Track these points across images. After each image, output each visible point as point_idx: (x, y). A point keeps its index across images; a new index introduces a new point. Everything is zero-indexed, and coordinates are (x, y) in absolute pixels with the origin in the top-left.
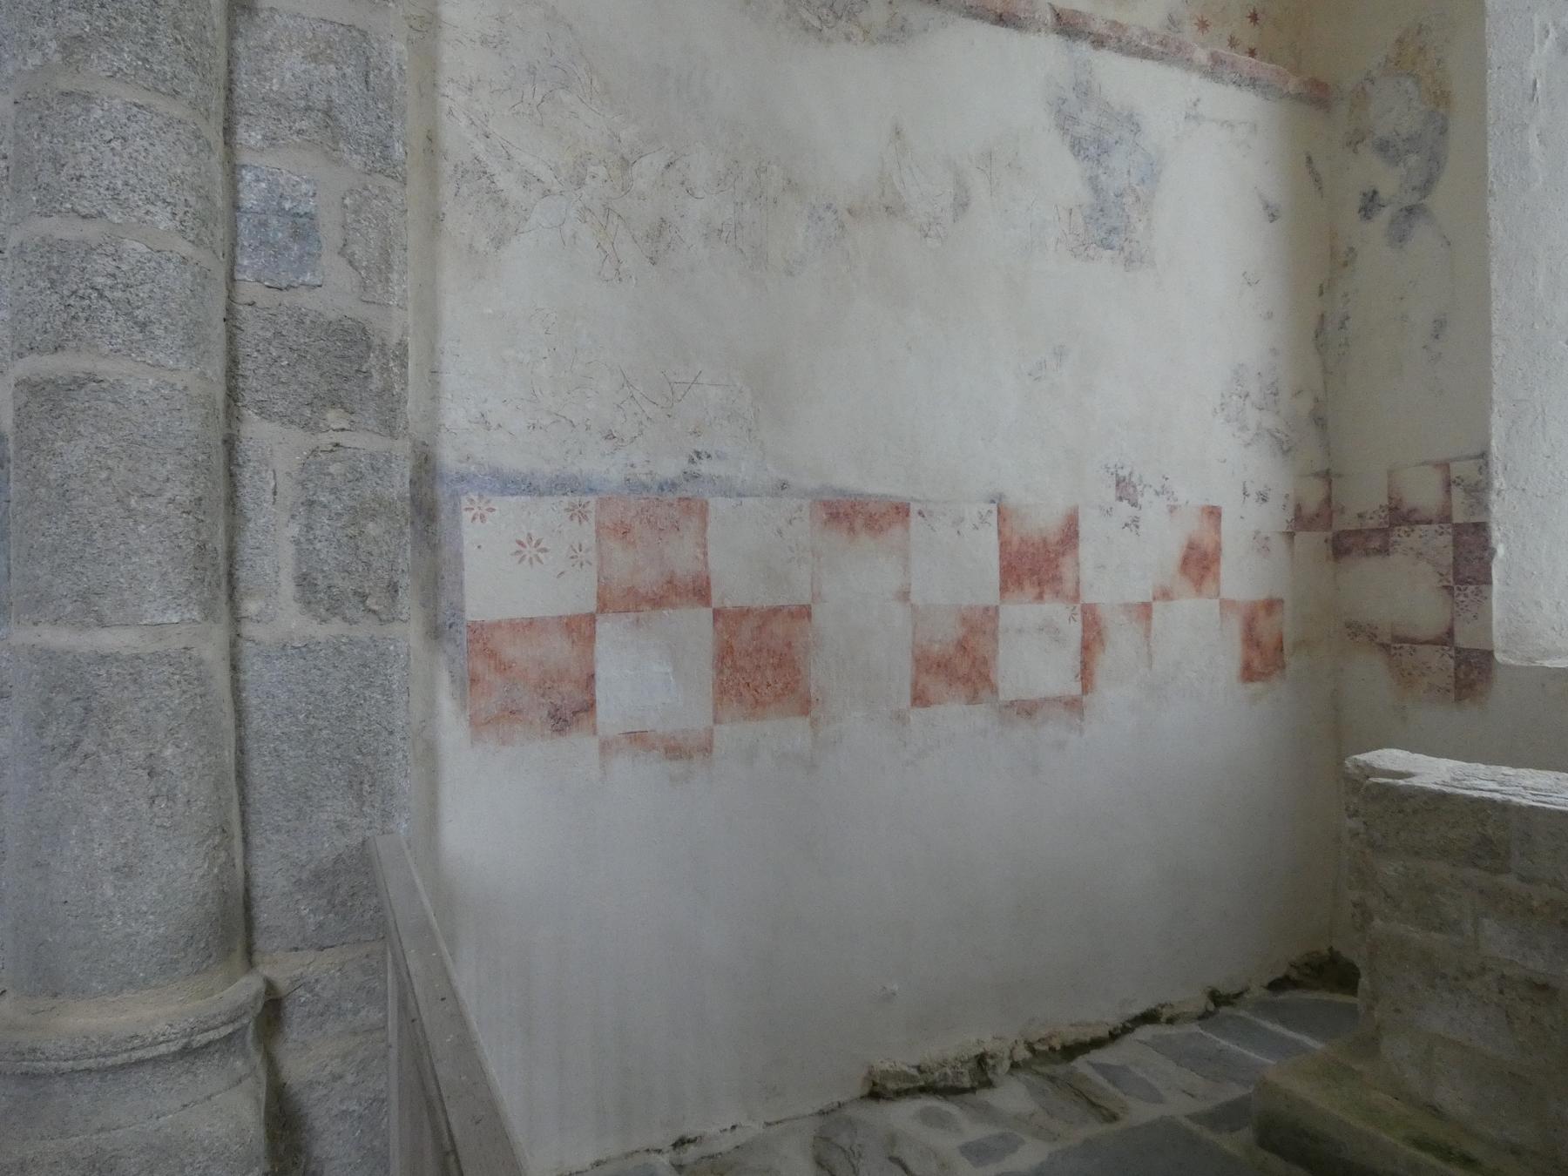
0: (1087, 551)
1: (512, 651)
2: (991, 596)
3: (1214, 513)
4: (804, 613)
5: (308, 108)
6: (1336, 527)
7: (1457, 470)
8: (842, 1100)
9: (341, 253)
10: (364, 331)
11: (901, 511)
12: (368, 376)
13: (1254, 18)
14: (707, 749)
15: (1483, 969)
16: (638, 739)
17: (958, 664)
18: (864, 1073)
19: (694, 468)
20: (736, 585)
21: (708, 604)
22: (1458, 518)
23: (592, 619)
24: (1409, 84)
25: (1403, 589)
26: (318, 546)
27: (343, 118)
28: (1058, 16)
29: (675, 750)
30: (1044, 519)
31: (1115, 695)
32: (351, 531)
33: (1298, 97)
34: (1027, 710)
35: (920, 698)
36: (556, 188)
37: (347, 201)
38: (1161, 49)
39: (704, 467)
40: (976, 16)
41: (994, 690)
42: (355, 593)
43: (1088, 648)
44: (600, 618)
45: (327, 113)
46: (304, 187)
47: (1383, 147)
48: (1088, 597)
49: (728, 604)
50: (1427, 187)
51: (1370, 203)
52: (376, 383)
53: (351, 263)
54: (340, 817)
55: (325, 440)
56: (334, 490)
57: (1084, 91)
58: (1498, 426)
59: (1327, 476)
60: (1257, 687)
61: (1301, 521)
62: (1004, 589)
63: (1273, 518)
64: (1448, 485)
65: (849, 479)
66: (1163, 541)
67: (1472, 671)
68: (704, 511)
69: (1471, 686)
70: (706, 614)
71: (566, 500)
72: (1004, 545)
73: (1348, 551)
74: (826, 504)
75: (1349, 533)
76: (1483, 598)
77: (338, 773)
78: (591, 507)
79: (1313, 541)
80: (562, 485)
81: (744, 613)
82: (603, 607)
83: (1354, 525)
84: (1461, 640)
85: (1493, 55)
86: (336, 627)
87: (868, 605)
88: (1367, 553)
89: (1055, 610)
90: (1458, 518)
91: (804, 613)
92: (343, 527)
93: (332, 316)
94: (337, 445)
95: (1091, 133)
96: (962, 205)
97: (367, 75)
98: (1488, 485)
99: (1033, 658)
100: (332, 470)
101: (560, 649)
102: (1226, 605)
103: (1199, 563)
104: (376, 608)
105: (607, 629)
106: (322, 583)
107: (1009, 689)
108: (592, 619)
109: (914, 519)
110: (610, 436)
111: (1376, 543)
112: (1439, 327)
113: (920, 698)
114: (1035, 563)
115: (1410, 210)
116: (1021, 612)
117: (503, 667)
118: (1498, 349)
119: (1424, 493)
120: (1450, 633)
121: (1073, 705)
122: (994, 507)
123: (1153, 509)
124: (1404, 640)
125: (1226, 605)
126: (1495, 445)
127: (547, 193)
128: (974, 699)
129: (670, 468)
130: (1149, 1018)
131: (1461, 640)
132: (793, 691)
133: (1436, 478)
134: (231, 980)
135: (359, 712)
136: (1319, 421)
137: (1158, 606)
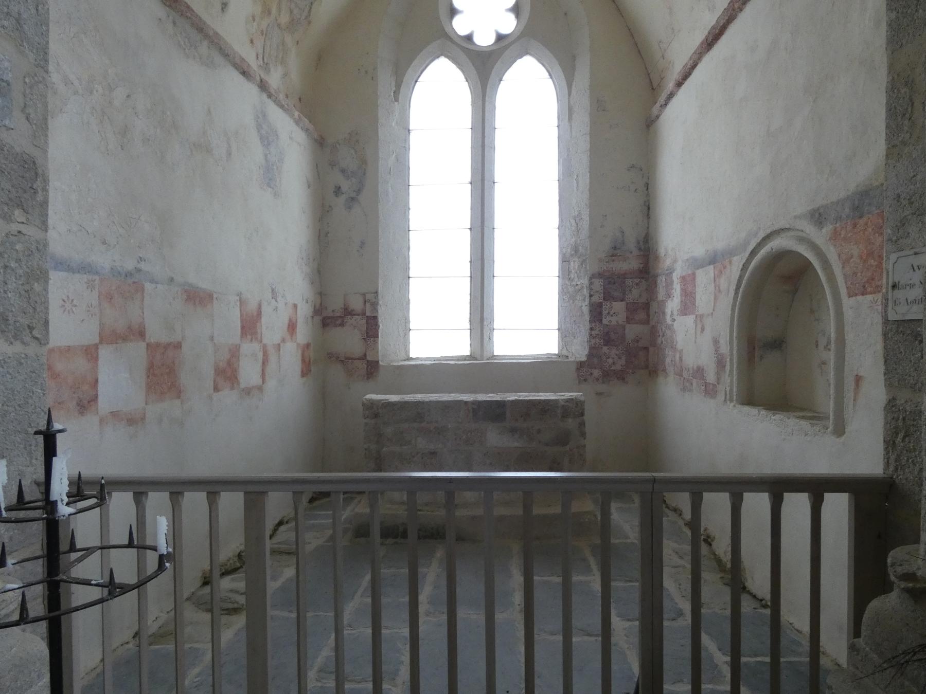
0: (264, 320)
1: (59, 366)
2: (237, 339)
3: (295, 306)
4: (178, 346)
5: (8, 14)
6: (327, 318)
7: (368, 297)
8: (193, 590)
9: (23, 111)
10: (34, 163)
11: (210, 296)
12: (36, 192)
13: (300, 99)
14: (143, 419)
15: (418, 453)
16: (115, 415)
17: (227, 374)
19: (139, 266)
20: (156, 333)
21: (144, 340)
22: (368, 314)
23: (96, 347)
24: (353, 151)
25: (348, 340)
26: (10, 295)
27: (26, 27)
28: (261, 80)
30: (252, 307)
31: (271, 384)
32: (27, 287)
33: (316, 140)
34: (248, 391)
35: (216, 389)
36: (80, 91)
37: (27, 80)
39: (142, 266)
40: (236, 68)
41: (238, 384)
42: (29, 326)
43: (265, 362)
44: (100, 346)
45: (18, 21)
46: (7, 64)
47: (343, 171)
48: (265, 341)
49: (152, 340)
50: (359, 191)
51: (338, 191)
52: (40, 197)
53: (28, 119)
54: (21, 467)
55: (14, 227)
56: (18, 261)
57: (264, 116)
58: (380, 282)
60: (305, 379)
62: (242, 337)
64: (365, 302)
67: (372, 368)
68: (143, 290)
69: (372, 374)
70: (143, 345)
71: (85, 277)
72: (242, 315)
73: (328, 325)
74: (186, 291)
75: (329, 318)
76: (376, 342)
77: (19, 440)
78: (96, 282)
79: (318, 319)
80: (85, 268)
81: (158, 345)
82: (101, 342)
83: (331, 315)
84: (369, 358)
85: (380, 154)
86: (18, 348)
88: (336, 326)
89: (255, 347)
90: (368, 314)
92: (22, 285)
93: (18, 149)
94: (20, 232)
97: (37, 6)
98: (377, 304)
100: (17, 247)
101: (80, 364)
102: (298, 345)
103: (292, 327)
104: (38, 336)
105: (105, 353)
106: (11, 319)
108: (96, 347)
109: (215, 301)
110: (104, 243)
111: (339, 322)
112: (362, 245)
113: (216, 389)
114: (250, 325)
115: (353, 199)
116: (249, 348)
117: (55, 376)
118: (380, 257)
119: (356, 304)
120: (365, 355)
121: (260, 389)
122: (238, 298)
124: (349, 358)
125: (298, 345)
126: (380, 289)
127: (76, 93)
128: (232, 388)
129: (130, 265)
130: (280, 523)
131: (369, 358)
133: (361, 299)
135: (30, 401)
136: (319, 272)
137: (282, 345)
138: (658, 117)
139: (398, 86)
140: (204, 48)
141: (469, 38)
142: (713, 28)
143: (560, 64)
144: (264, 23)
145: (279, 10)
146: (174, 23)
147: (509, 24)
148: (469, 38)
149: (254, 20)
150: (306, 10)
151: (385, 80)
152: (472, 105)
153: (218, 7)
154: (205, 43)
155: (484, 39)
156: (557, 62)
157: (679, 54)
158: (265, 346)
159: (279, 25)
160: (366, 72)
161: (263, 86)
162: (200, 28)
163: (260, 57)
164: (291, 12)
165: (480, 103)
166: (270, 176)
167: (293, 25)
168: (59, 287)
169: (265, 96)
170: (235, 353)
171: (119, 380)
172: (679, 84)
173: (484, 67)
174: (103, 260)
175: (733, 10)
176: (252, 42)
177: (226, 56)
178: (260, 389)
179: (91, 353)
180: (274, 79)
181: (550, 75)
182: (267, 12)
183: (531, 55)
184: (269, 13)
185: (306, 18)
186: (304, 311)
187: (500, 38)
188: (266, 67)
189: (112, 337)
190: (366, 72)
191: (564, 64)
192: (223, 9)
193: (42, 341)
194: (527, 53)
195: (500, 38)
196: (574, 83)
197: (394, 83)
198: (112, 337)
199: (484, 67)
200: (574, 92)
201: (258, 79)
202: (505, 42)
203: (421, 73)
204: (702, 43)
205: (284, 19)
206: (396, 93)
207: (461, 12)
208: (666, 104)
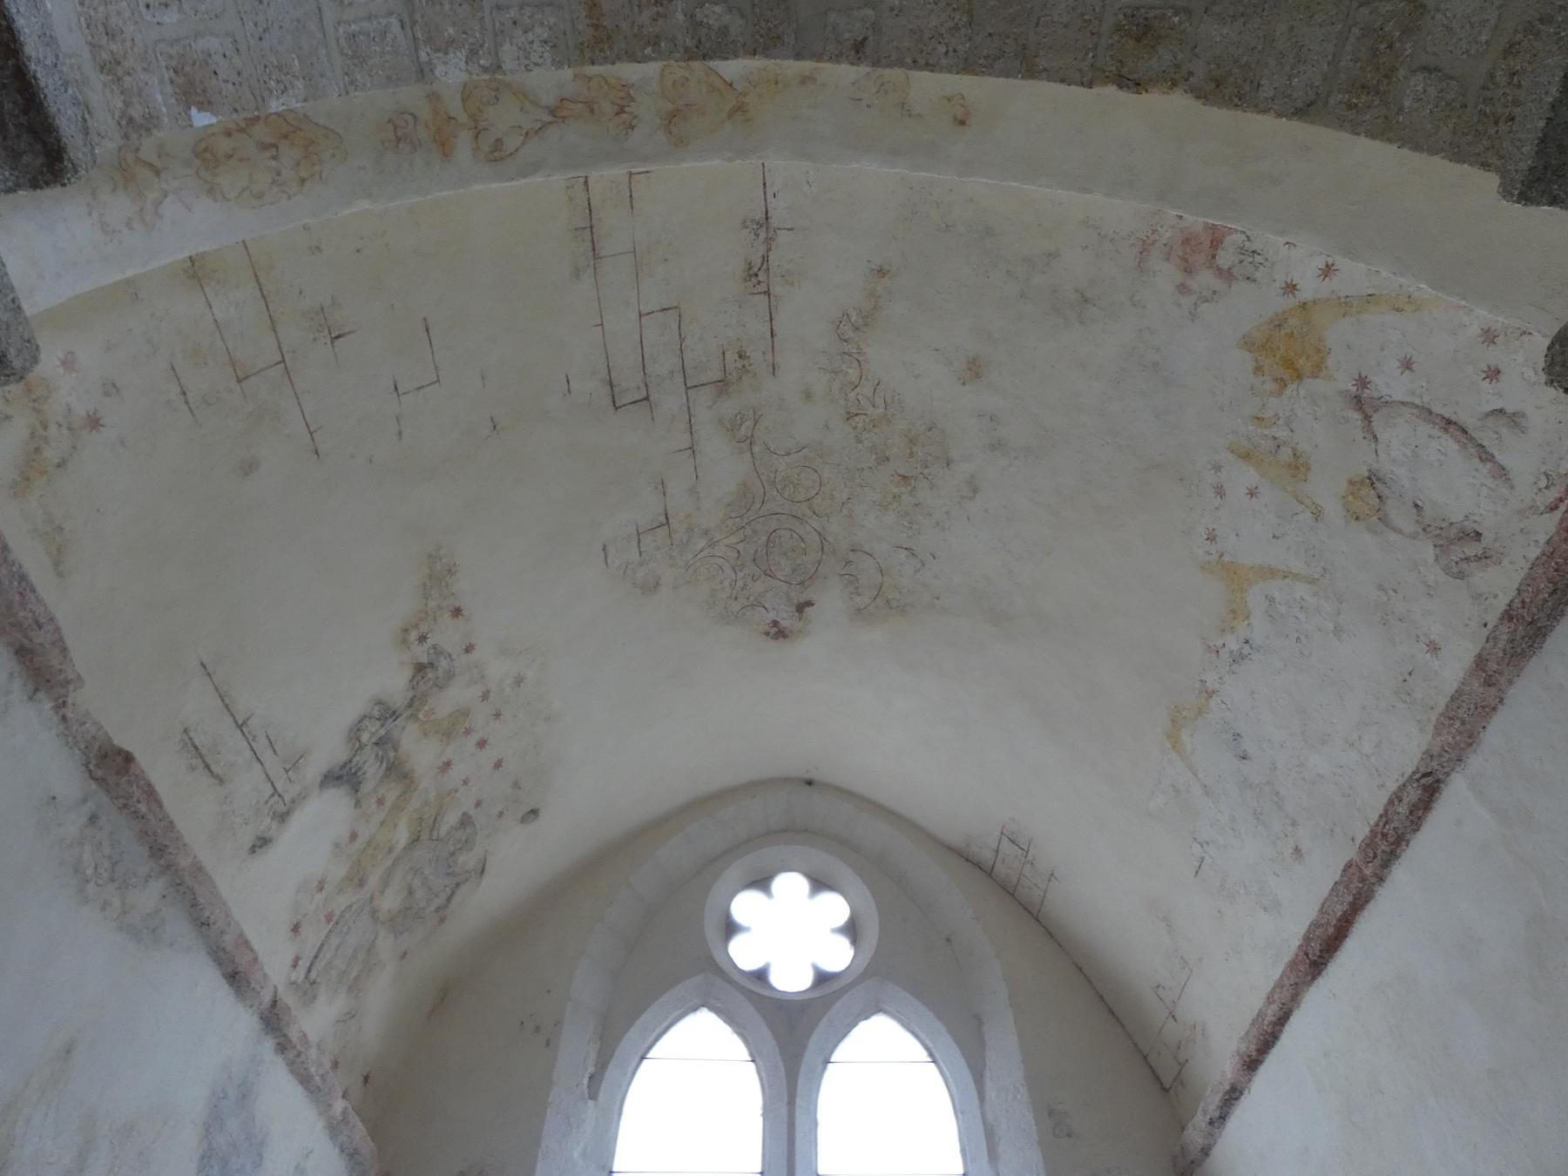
11: (253, 850)
13: (366, 1079)
28: (274, 1003)
40: (219, 962)
57: (245, 1094)
138: (1206, 1151)
139: (602, 1065)
140: (149, 896)
141: (761, 975)
142: (1315, 925)
143: (950, 1032)
144: (342, 901)
145: (385, 883)
146: (93, 819)
147: (839, 956)
148: (761, 975)
149: (321, 889)
150: (443, 897)
151: (575, 1048)
152: (763, 1115)
153: (247, 839)
154: (158, 885)
155: (791, 979)
156: (943, 1029)
157: (1217, 1003)
159: (374, 913)
160: (538, 1029)
161: (273, 1020)
162: (160, 845)
163: (304, 964)
164: (411, 892)
165: (784, 1111)
167: (401, 921)
169: (269, 1044)
172: (1252, 1064)
173: (790, 1036)
175: (1363, 880)
176: (296, 928)
177: (158, 851)
180: (315, 1022)
181: (931, 1055)
182: (357, 879)
183: (886, 1012)
184: (362, 883)
185: (438, 910)
187: (822, 978)
188: (308, 990)
190: (538, 1029)
191: (959, 1034)
192: (253, 850)
194: (878, 1009)
195: (822, 978)
196: (987, 1073)
197: (593, 1056)
199: (790, 1036)
200: (991, 1093)
201: (267, 997)
202: (836, 986)
203: (656, 1040)
204: (1293, 965)
205: (390, 902)
206: (595, 1080)
207: (747, 929)
208: (1223, 1118)
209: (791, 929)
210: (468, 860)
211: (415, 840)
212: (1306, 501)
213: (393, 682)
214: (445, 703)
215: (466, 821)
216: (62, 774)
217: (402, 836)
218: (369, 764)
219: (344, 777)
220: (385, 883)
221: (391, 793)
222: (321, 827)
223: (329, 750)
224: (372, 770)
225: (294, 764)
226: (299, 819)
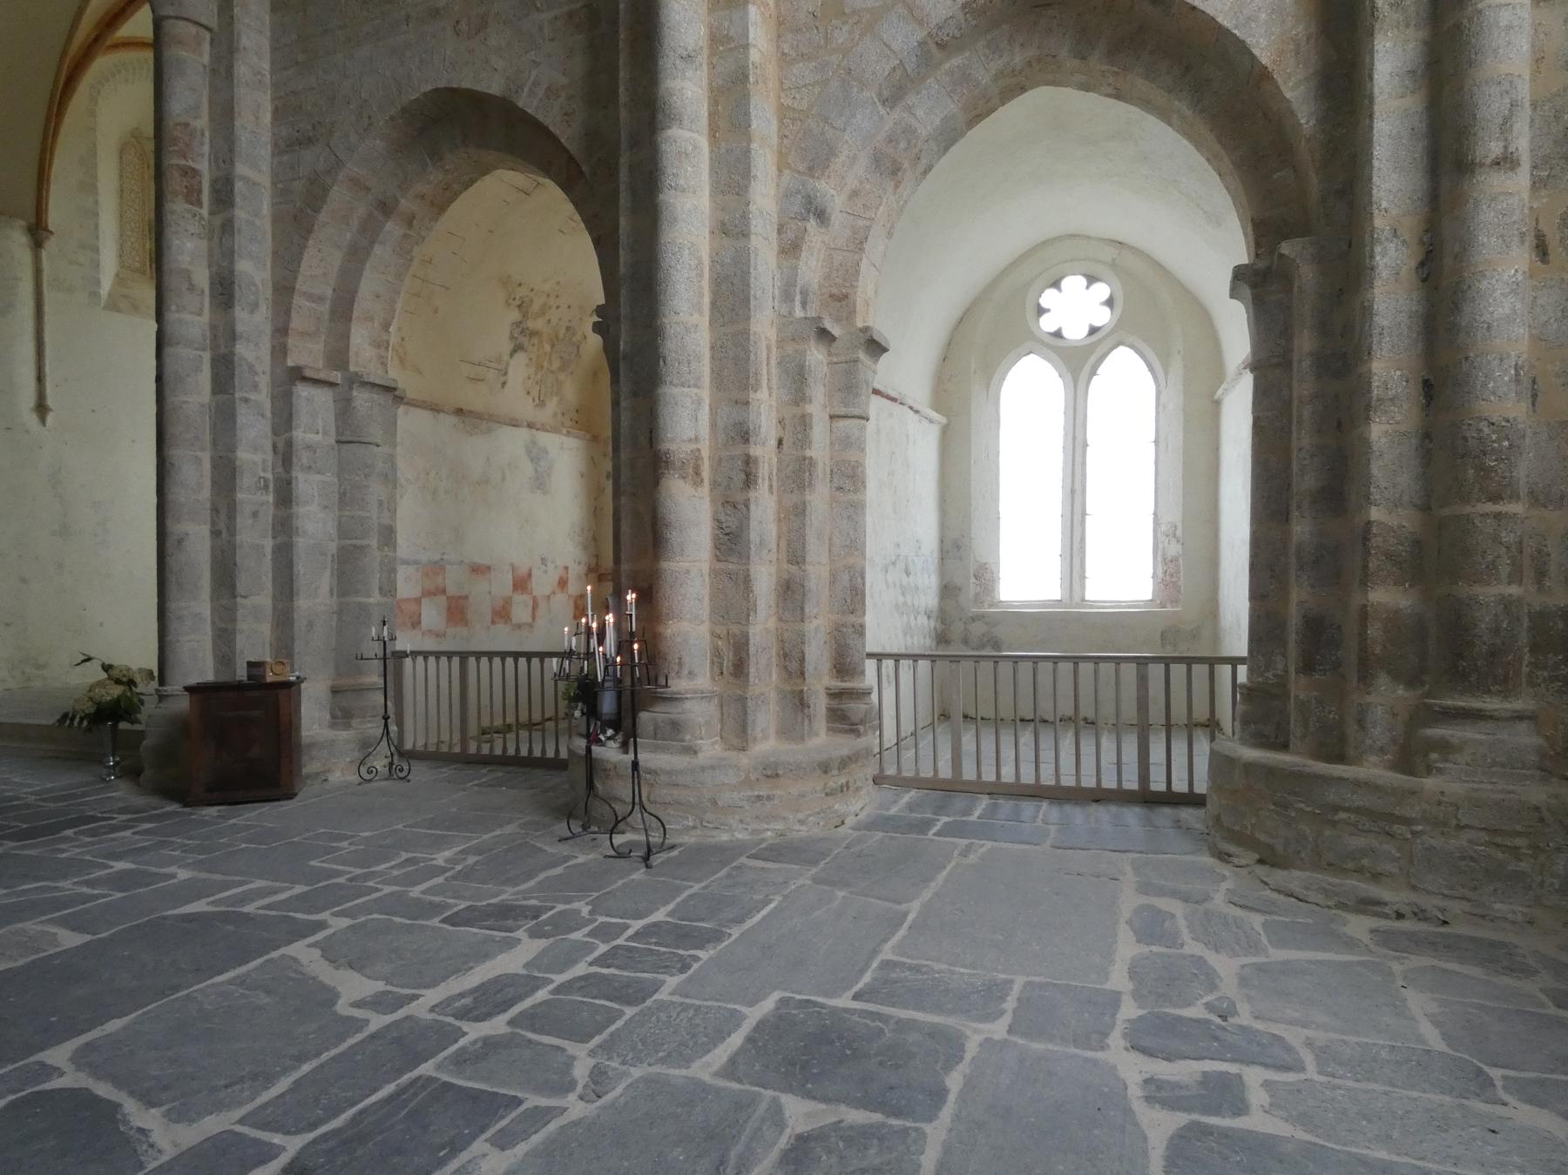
4: (466, 597)
11: (489, 568)
16: (430, 631)
17: (502, 613)
18: (892, 347)
20: (452, 590)
29: (438, 635)
30: (523, 571)
31: (540, 622)
34: (519, 626)
35: (493, 622)
38: (555, 430)
43: (534, 608)
57: (534, 443)
59: (597, 556)
61: (590, 570)
63: (582, 569)
65: (477, 560)
66: (554, 576)
80: (416, 562)
87: (483, 594)
91: (466, 597)
95: (536, 454)
96: (504, 479)
99: (521, 613)
103: (563, 583)
107: (514, 621)
113: (493, 622)
116: (519, 598)
121: (531, 626)
123: (551, 567)
129: (438, 557)
132: (410, 225)
134: (1437, 1024)
136: (594, 539)
155: (1075, 332)
158: (535, 600)
162: (479, 416)
166: (540, 483)
168: (402, 572)
170: (507, 602)
171: (432, 615)
173: (1078, 362)
174: (424, 557)
178: (531, 626)
179: (418, 601)
186: (576, 571)
187: (1093, 330)
189: (428, 593)
193: (394, 596)
195: (1093, 330)
198: (428, 593)
199: (1078, 362)
205: (556, 364)
209: (1076, 306)
210: (578, 337)
211: (553, 346)
212: (281, 446)
213: (515, 315)
214: (536, 307)
215: (568, 328)
216: (453, 419)
217: (547, 348)
218: (522, 337)
219: (518, 348)
220: (550, 362)
221: (535, 340)
222: (519, 368)
223: (507, 346)
224: (524, 340)
225: (499, 360)
226: (510, 373)
